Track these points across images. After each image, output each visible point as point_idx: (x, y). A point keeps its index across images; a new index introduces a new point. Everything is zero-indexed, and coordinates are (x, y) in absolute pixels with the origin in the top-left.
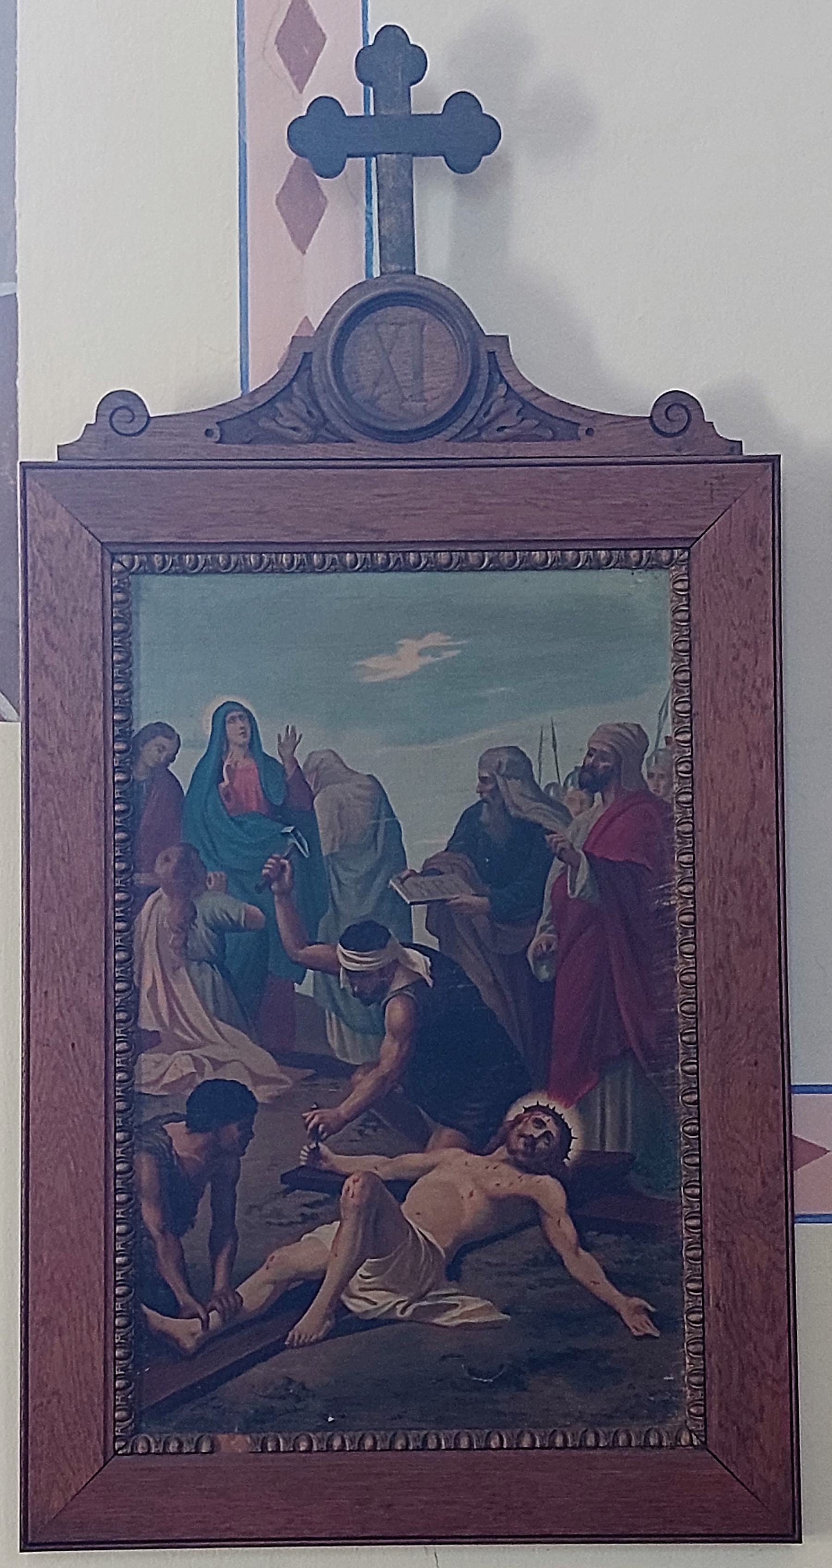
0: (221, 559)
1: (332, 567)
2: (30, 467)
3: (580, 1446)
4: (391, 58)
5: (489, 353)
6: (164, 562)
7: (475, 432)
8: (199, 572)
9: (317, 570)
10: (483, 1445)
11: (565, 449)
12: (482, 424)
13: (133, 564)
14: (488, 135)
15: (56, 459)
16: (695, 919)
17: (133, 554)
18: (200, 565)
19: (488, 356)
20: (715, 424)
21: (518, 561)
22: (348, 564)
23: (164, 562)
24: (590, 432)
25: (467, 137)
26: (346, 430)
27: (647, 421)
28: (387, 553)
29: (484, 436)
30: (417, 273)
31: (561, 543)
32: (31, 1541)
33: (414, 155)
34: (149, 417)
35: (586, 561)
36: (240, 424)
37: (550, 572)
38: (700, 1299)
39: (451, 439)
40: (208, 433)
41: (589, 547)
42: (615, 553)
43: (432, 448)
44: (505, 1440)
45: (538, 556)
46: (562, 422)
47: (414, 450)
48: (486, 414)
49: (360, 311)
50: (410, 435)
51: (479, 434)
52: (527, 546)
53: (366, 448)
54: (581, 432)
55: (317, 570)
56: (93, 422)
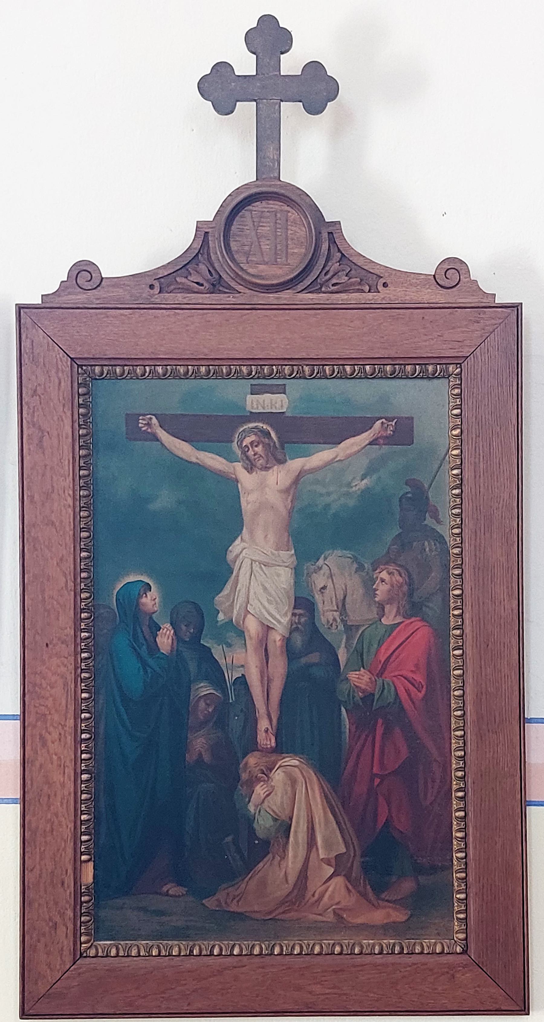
0: (138, 370)
1: (129, 375)
2: (23, 308)
3: (190, 955)
4: (269, 37)
5: (329, 233)
9: (119, 378)
10: (270, 952)
13: (334, 371)
14: (205, 87)
15: (40, 302)
16: (462, 491)
19: (328, 235)
21: (438, 372)
24: (152, 287)
25: (317, 89)
27: (432, 278)
29: (323, 289)
33: (282, 101)
34: (102, 278)
35: (420, 372)
36: (165, 279)
37: (335, 380)
38: (460, 559)
40: (385, 285)
43: (286, 296)
46: (368, 276)
47: (272, 298)
48: (325, 274)
49: (239, 206)
50: (271, 250)
51: (321, 288)
52: (444, 361)
53: (247, 296)
54: (157, 285)
55: (119, 378)
56: (66, 279)
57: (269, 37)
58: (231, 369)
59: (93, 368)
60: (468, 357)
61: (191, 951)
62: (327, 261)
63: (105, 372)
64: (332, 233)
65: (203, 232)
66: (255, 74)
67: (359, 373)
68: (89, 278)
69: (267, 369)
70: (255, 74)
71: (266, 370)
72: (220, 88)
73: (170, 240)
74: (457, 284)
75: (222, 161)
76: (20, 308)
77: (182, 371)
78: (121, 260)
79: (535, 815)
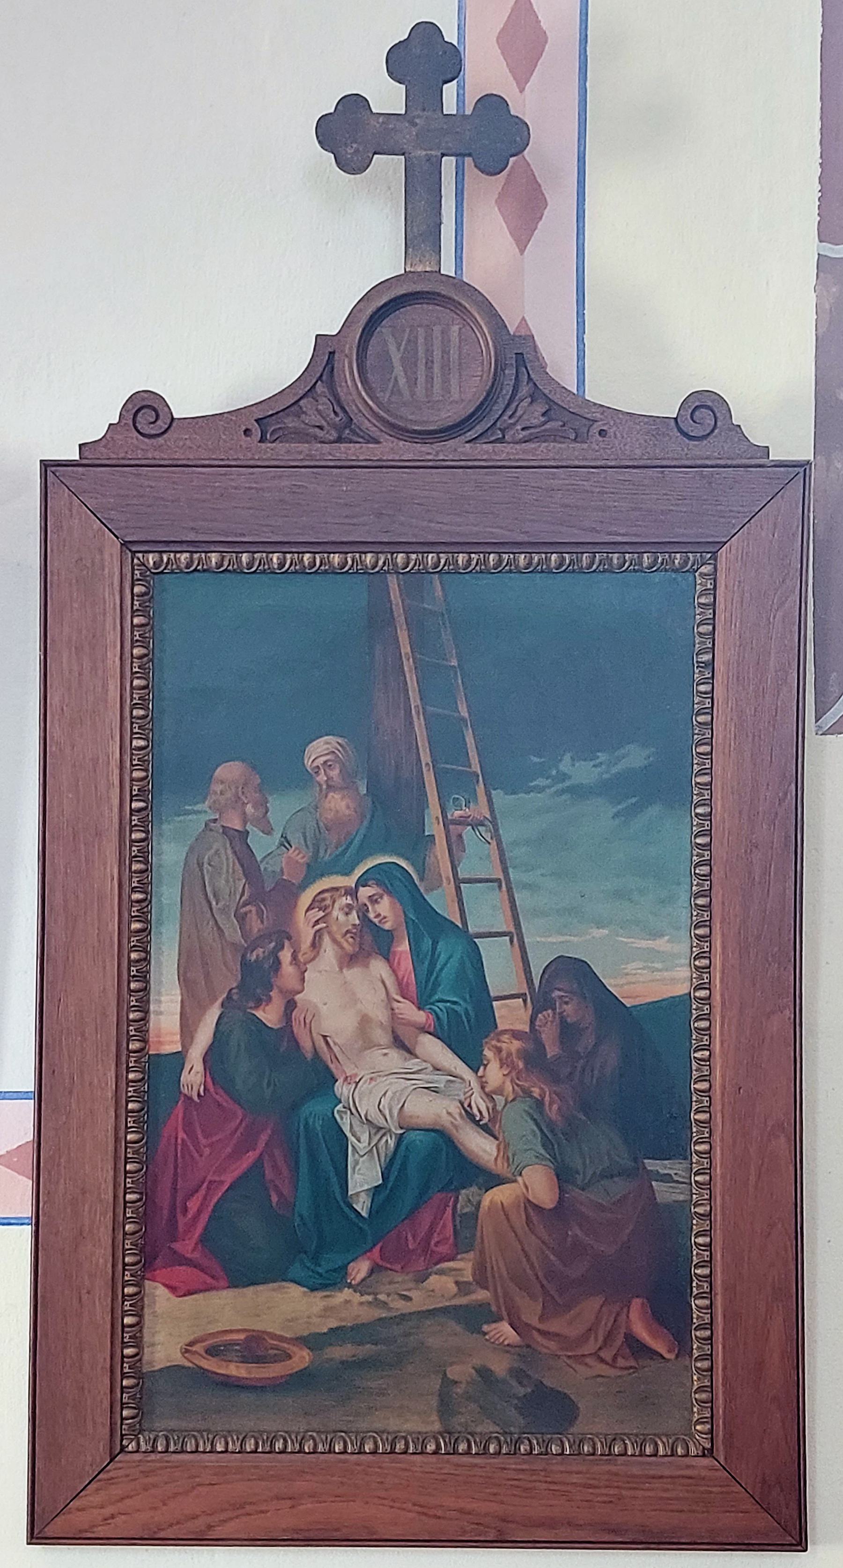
6: (500, 561)
7: (497, 434)
8: (315, 572)
9: (554, 571)
11: (571, 451)
12: (505, 425)
13: (686, 562)
15: (77, 458)
17: (378, 553)
18: (534, 565)
20: (742, 427)
22: (369, 566)
23: (500, 561)
26: (374, 432)
27: (672, 422)
28: (438, 553)
30: (442, 272)
31: (392, 546)
32: (39, 1533)
34: (173, 419)
36: (269, 421)
39: (467, 442)
41: (294, 550)
42: (196, 556)
43: (458, 448)
44: (411, 1444)
45: (336, 559)
46: (573, 419)
48: (510, 417)
49: (383, 309)
53: (391, 448)
57: (423, 58)
58: (564, 559)
59: (178, 555)
60: (726, 543)
61: (272, 1445)
62: (518, 396)
63: (443, 561)
64: (522, 354)
65: (326, 350)
66: (445, 113)
67: (569, 566)
68: (153, 420)
69: (402, 558)
70: (403, 112)
71: (646, 559)
72: (347, 133)
73: (281, 365)
74: (712, 431)
75: (345, 247)
76: (46, 465)
77: (214, 561)
78: (196, 393)
79: (824, 754)
